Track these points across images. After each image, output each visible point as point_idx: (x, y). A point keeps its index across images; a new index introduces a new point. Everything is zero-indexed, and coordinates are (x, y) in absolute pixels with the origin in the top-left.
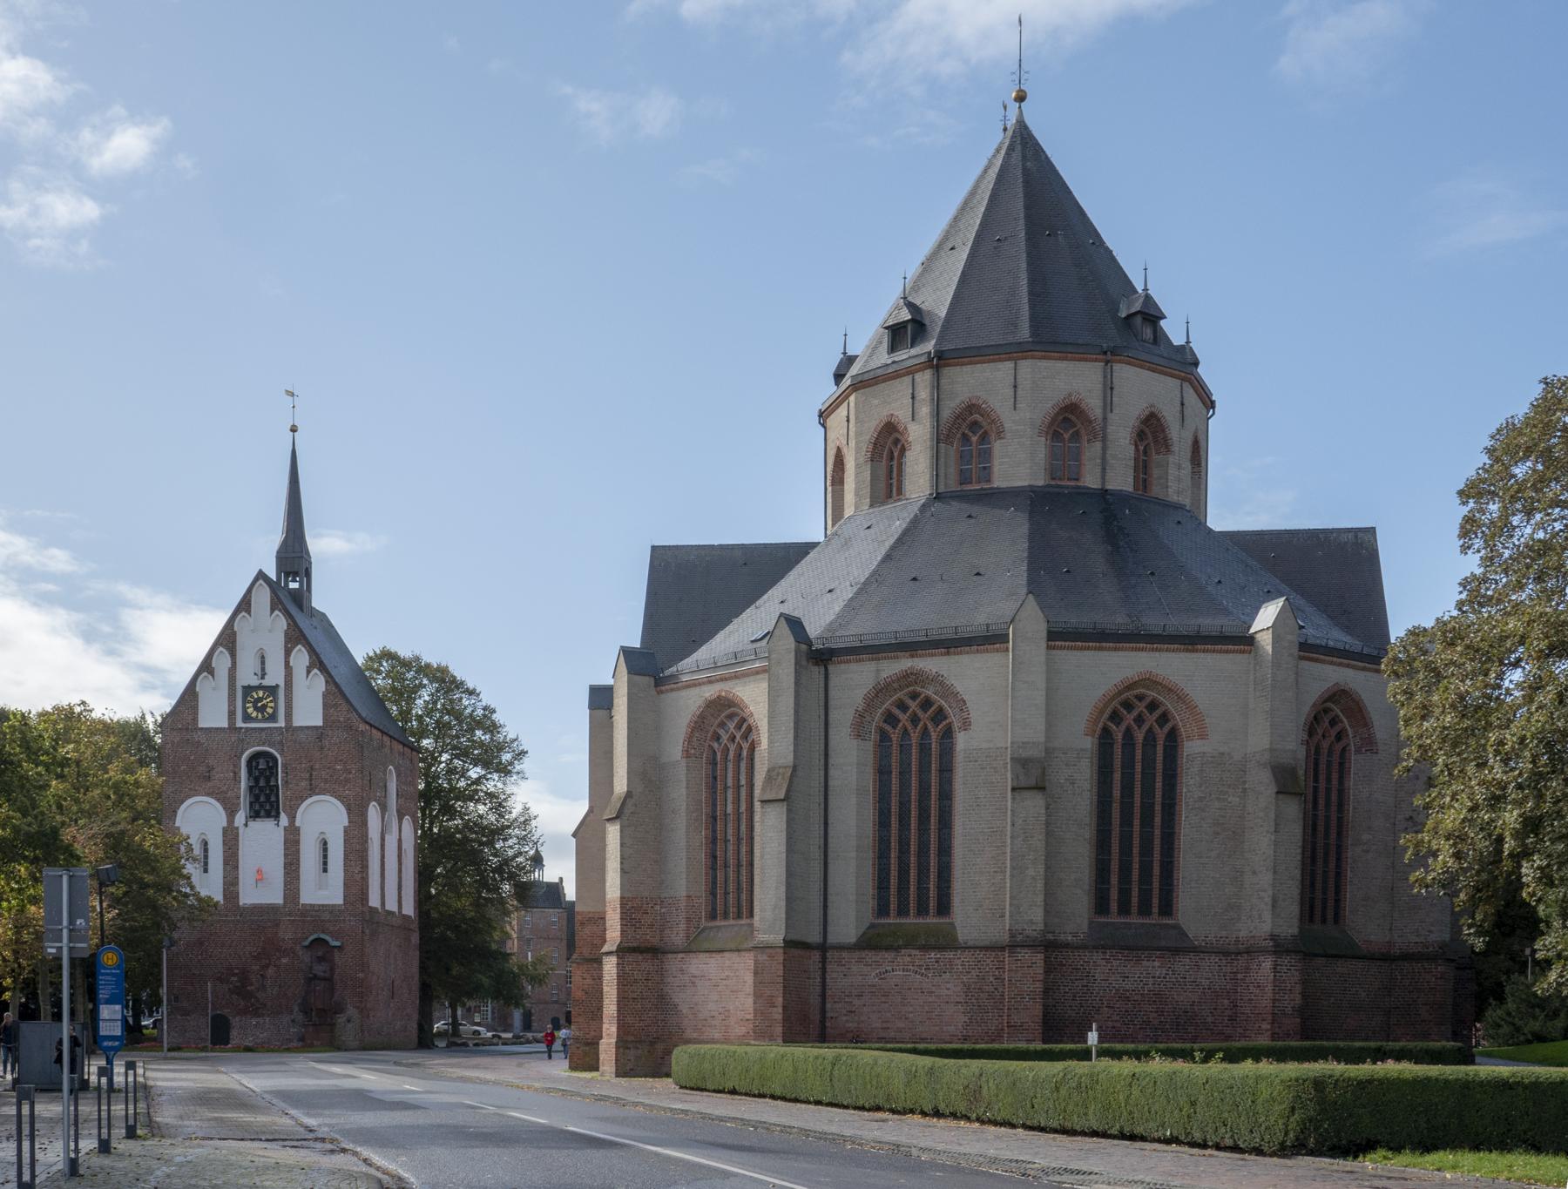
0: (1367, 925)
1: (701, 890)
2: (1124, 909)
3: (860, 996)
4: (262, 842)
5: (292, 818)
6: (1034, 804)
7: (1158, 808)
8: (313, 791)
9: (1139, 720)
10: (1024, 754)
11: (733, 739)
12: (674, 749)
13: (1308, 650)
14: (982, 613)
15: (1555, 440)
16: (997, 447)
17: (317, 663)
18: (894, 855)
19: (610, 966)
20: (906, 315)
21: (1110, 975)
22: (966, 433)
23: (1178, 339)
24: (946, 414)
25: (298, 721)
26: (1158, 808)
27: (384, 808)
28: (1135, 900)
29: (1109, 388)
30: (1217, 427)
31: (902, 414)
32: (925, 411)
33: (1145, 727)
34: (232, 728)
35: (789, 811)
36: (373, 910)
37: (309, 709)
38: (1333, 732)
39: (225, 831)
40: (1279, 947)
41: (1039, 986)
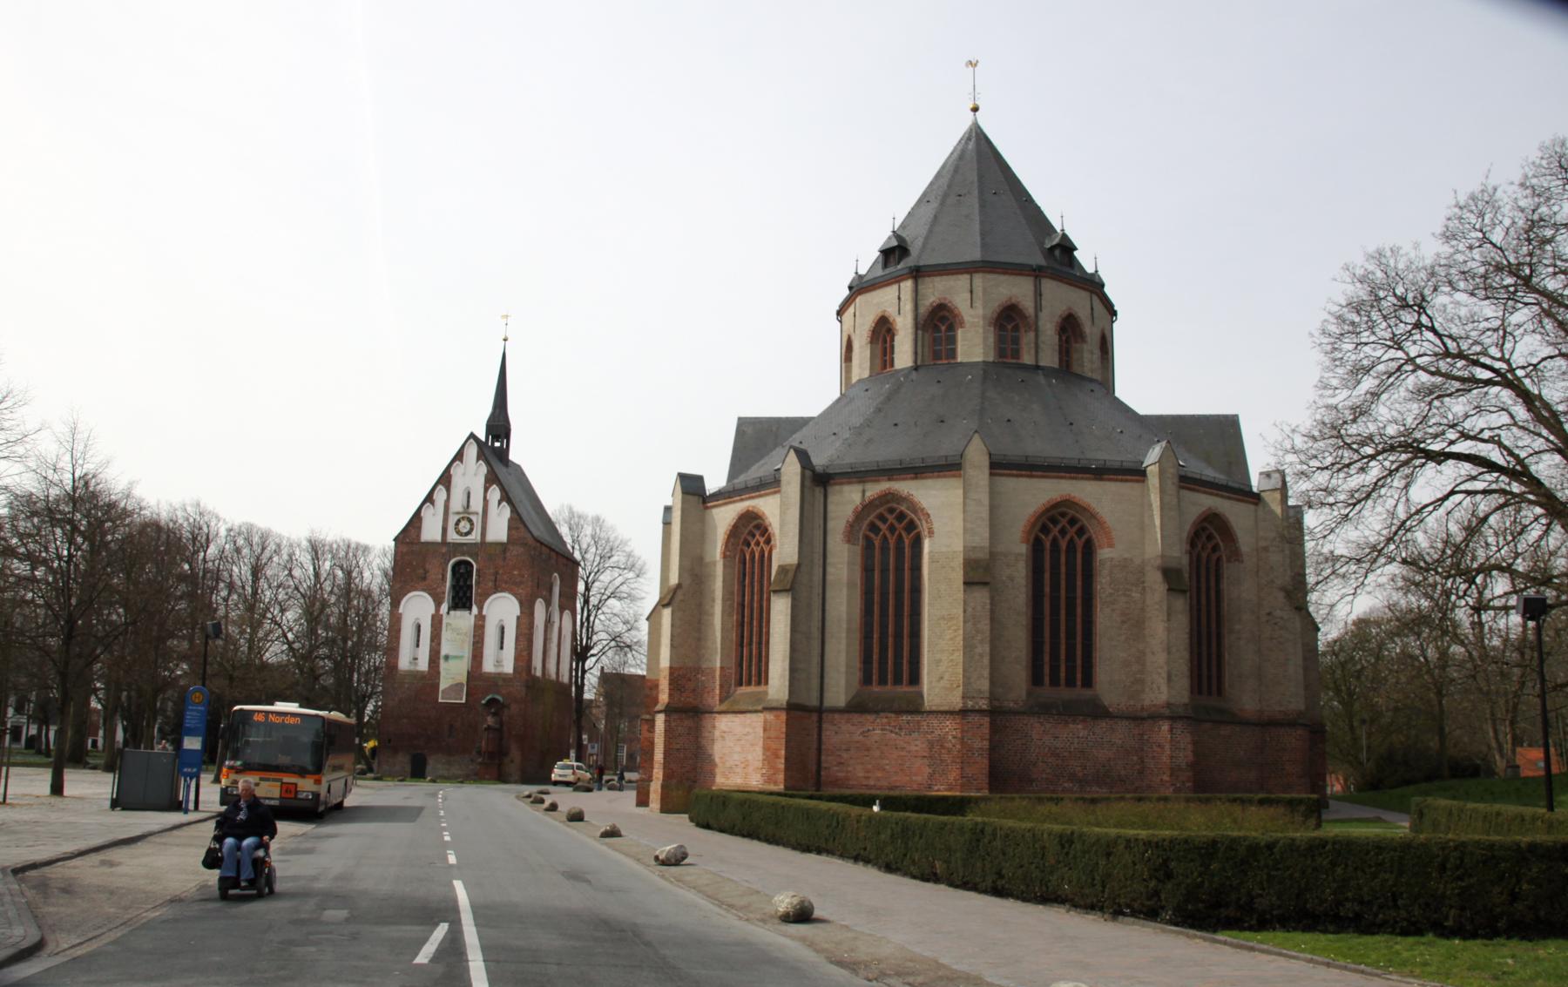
0: (1247, 700)
1: (732, 663)
2: (1055, 682)
3: (848, 750)
4: (462, 621)
5: (481, 608)
6: (981, 596)
7: (1079, 601)
8: (496, 589)
9: (1063, 532)
10: (973, 556)
11: (758, 544)
12: (716, 550)
13: (1188, 482)
14: (945, 447)
15: (1534, 533)
16: (960, 332)
17: (506, 497)
18: (876, 636)
19: (660, 720)
20: (895, 243)
21: (1047, 739)
22: (937, 324)
23: (1090, 269)
24: (922, 310)
25: (490, 538)
26: (1079, 601)
27: (548, 603)
28: (1063, 675)
29: (1038, 294)
30: (1117, 327)
31: (891, 311)
32: (908, 307)
33: (1068, 537)
34: (444, 542)
35: (794, 599)
36: (535, 678)
37: (498, 529)
38: (1210, 546)
39: (433, 617)
40: (1173, 715)
41: (986, 744)
